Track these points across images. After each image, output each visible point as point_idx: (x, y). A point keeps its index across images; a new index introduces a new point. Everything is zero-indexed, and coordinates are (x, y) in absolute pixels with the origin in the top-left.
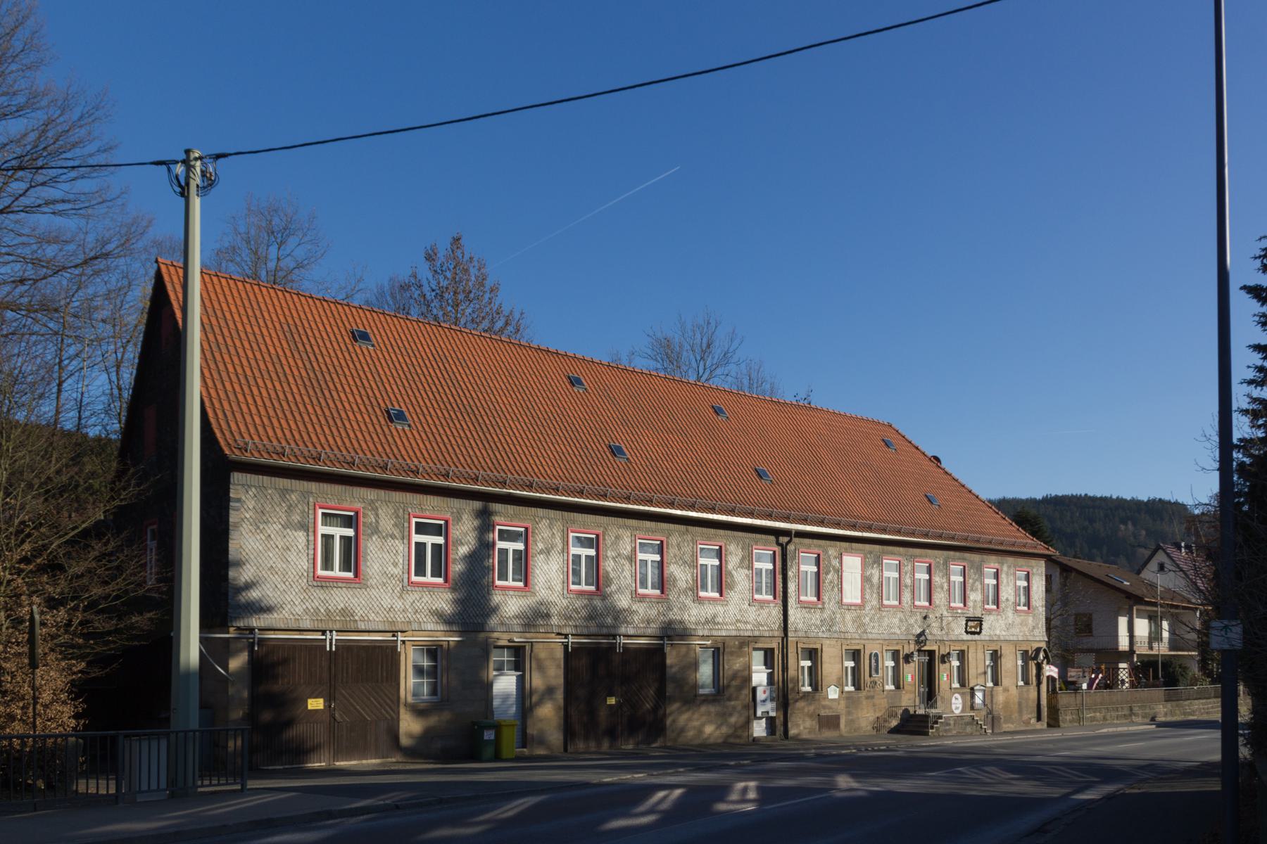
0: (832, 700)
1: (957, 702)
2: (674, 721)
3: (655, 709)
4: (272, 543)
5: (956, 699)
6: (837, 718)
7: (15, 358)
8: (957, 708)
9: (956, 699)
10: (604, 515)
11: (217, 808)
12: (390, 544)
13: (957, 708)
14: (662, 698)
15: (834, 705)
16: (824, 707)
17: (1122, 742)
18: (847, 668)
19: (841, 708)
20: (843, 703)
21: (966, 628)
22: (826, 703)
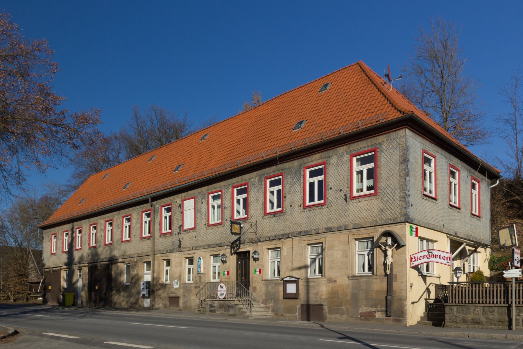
0: (176, 288)
1: (222, 289)
2: (317, 294)
3: (105, 294)
4: (384, 214)
5: (222, 287)
6: (177, 298)
7: (371, 112)
8: (222, 294)
9: (222, 287)
10: (436, 145)
11: (141, 314)
12: (355, 206)
13: (222, 294)
14: (110, 289)
15: (176, 291)
16: (172, 293)
17: (132, 321)
18: (450, 260)
19: (180, 294)
20: (182, 290)
21: (231, 230)
22: (172, 290)
